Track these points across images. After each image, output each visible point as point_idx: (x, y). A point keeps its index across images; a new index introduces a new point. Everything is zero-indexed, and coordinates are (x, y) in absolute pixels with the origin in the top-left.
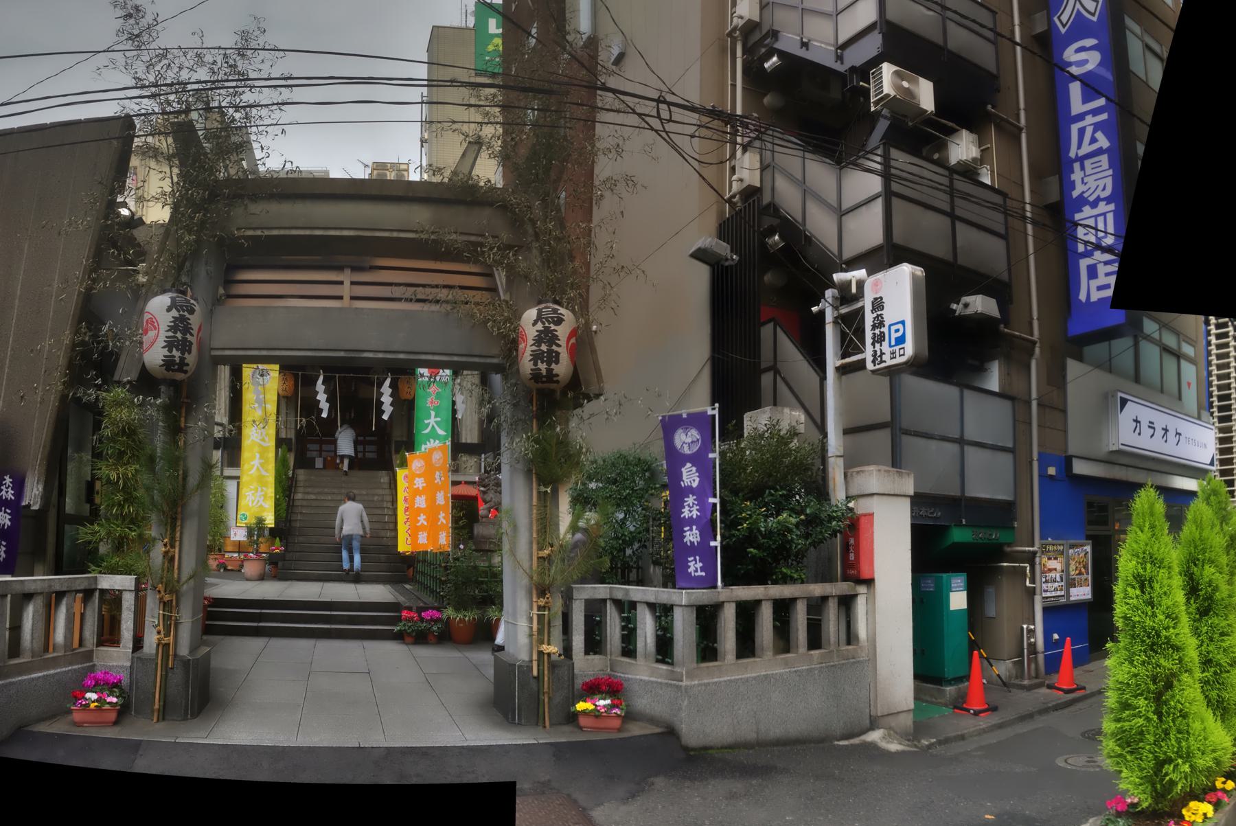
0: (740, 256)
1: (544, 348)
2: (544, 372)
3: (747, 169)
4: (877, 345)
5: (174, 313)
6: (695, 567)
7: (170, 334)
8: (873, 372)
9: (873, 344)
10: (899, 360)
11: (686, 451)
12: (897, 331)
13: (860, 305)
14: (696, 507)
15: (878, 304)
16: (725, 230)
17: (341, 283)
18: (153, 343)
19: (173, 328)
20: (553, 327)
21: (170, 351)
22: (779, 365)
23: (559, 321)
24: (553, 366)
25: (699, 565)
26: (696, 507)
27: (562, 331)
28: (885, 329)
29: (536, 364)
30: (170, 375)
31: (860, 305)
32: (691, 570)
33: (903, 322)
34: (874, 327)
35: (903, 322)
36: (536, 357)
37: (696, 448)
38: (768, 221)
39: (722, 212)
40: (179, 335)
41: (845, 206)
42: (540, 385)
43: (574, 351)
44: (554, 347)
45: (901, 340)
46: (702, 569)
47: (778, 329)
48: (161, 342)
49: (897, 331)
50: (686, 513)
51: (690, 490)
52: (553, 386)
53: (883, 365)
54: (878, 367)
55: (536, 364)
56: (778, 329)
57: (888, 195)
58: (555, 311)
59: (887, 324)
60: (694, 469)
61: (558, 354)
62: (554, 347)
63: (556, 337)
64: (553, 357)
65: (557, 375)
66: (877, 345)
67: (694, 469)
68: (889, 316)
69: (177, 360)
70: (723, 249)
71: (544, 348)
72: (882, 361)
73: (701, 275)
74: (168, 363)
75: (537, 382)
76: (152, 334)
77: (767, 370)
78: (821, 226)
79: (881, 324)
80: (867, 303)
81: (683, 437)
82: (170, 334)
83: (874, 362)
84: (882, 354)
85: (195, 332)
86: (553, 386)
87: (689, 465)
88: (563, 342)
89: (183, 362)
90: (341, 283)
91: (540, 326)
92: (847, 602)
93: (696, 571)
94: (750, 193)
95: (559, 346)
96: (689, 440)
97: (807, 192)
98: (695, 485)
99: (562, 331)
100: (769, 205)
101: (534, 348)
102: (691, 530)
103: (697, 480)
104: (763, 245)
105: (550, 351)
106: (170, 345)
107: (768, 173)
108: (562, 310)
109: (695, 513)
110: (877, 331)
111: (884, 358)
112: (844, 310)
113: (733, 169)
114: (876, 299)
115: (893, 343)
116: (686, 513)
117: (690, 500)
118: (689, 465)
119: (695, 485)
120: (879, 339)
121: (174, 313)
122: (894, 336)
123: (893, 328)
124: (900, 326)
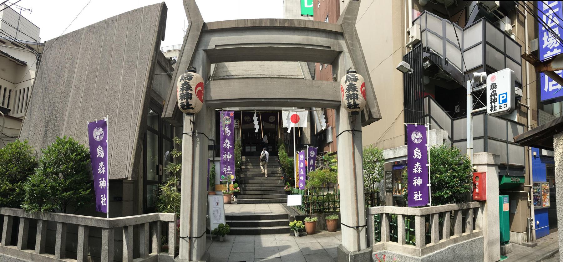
0: (414, 70)
1: (351, 92)
2: (353, 104)
3: (415, 33)
4: (493, 104)
6: (417, 196)
8: (490, 114)
9: (491, 103)
10: (503, 109)
11: (416, 142)
12: (503, 97)
13: (483, 87)
14: (420, 168)
15: (494, 86)
16: (405, 58)
20: (354, 83)
22: (431, 114)
23: (356, 80)
24: (356, 100)
25: (420, 195)
26: (420, 168)
27: (358, 84)
28: (497, 97)
29: (348, 101)
31: (483, 87)
32: (415, 198)
33: (506, 94)
34: (491, 96)
35: (506, 94)
36: (348, 97)
37: (420, 141)
38: (426, 55)
39: (403, 52)
41: (465, 48)
42: (352, 110)
43: (364, 94)
44: (355, 92)
45: (505, 101)
46: (421, 197)
47: (431, 100)
49: (503, 97)
50: (415, 171)
51: (417, 160)
52: (358, 110)
53: (496, 111)
54: (493, 112)
55: (348, 101)
56: (431, 100)
57: (485, 43)
58: (354, 76)
59: (498, 94)
60: (419, 150)
61: (191, 94)
62: (355, 92)
64: (355, 97)
65: (358, 105)
66: (493, 104)
68: (499, 91)
70: (408, 66)
71: (351, 92)
72: (495, 110)
73: (400, 74)
75: (350, 108)
77: (427, 116)
78: (453, 56)
79: (495, 94)
80: (488, 85)
83: (491, 110)
84: (495, 107)
86: (358, 110)
87: (417, 148)
88: (359, 89)
91: (348, 83)
92: (475, 211)
93: (418, 198)
94: (417, 43)
95: (357, 91)
96: (418, 137)
97: (445, 40)
98: (420, 158)
99: (358, 84)
100: (425, 48)
101: (347, 93)
102: (417, 179)
104: (421, 65)
105: (354, 94)
107: (424, 34)
108: (357, 75)
109: (420, 171)
110: (493, 98)
111: (496, 108)
112: (476, 89)
113: (409, 33)
114: (493, 84)
115: (501, 102)
116: (415, 171)
117: (418, 164)
118: (417, 148)
119: (420, 158)
120: (494, 101)
122: (501, 99)
123: (501, 96)
124: (505, 95)
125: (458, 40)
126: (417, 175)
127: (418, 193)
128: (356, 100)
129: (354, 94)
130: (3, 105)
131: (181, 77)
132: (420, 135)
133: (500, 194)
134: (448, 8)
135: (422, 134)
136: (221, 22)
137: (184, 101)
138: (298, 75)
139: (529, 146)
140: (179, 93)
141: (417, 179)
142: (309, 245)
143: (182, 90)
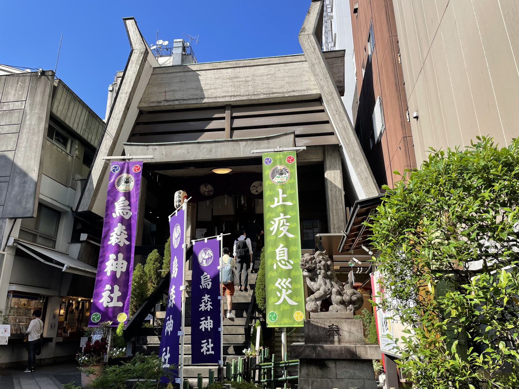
14: (209, 303)
17: (223, 118)
25: (211, 345)
26: (209, 303)
32: (204, 350)
50: (203, 307)
51: (206, 291)
90: (223, 118)
93: (208, 350)
98: (209, 287)
102: (206, 319)
109: (209, 307)
116: (203, 307)
117: (206, 297)
119: (209, 287)
125: (348, 118)
126: (206, 314)
127: (208, 342)
130: (223, 130)
133: (302, 248)
136: (355, 95)
138: (308, 89)
141: (206, 319)
142: (312, 15)
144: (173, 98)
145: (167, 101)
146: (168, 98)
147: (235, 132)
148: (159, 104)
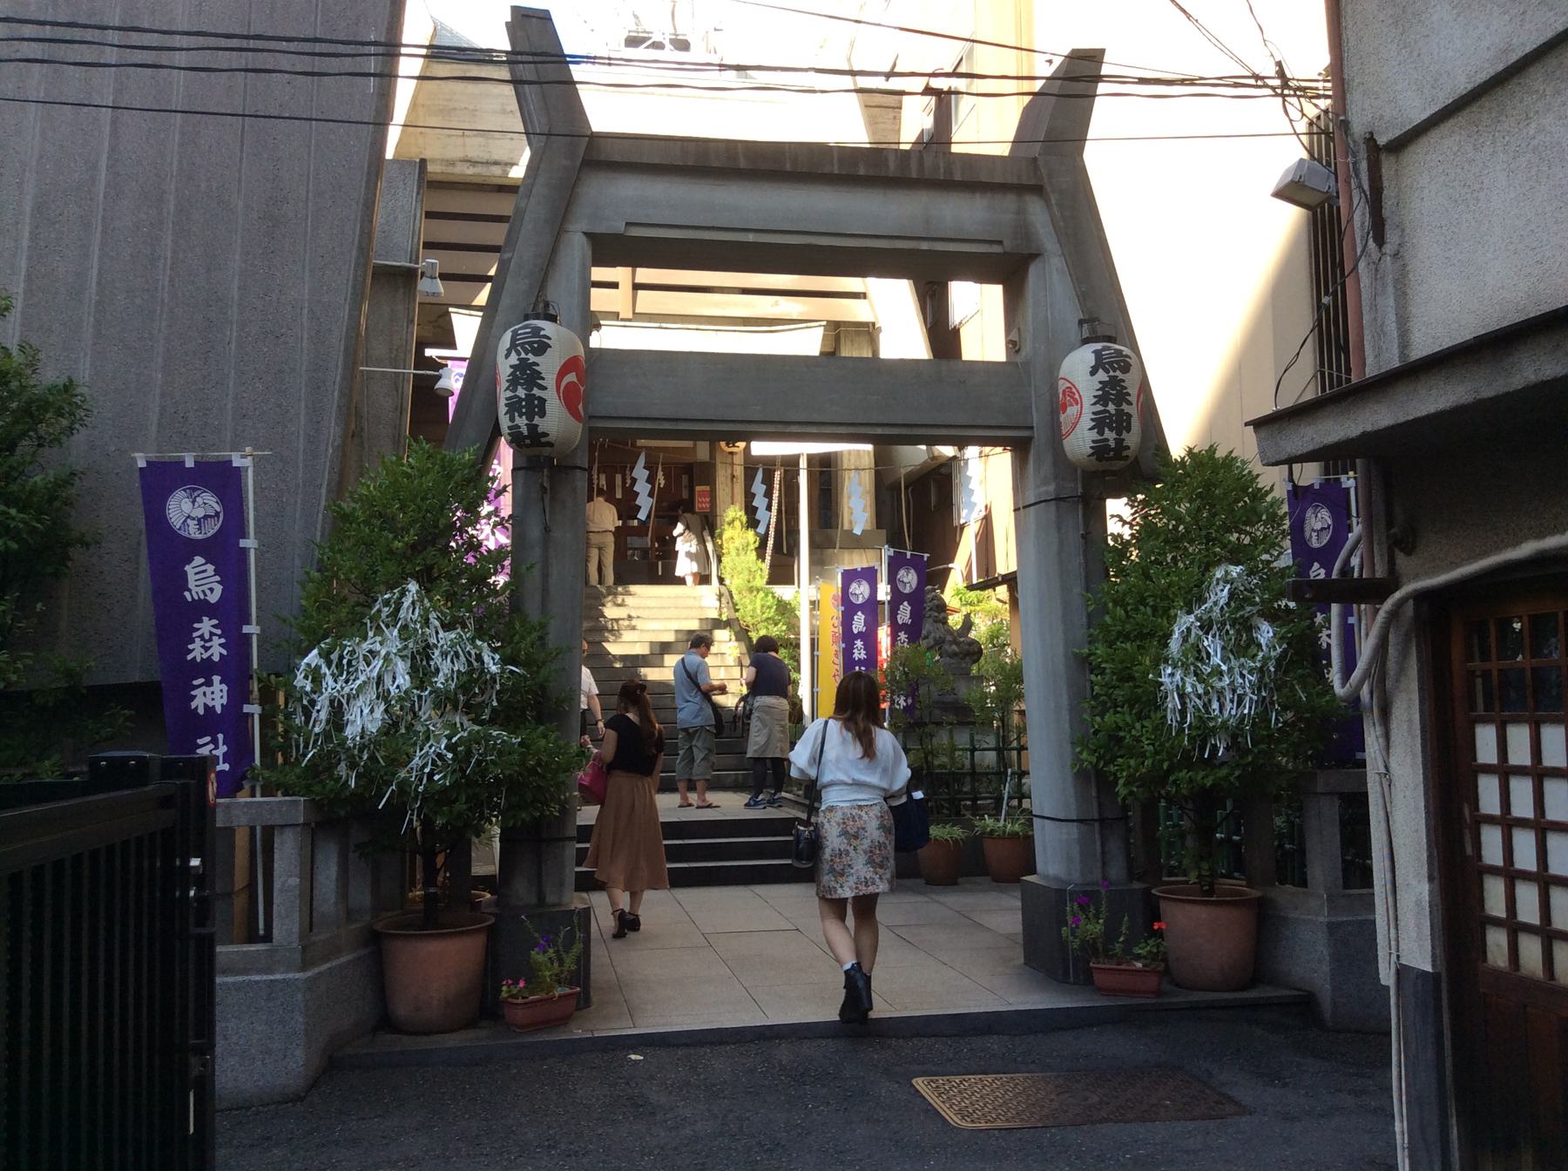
5: (1102, 375)
7: (1099, 408)
11: (193, 532)
18: (1075, 424)
19: (1102, 399)
20: (532, 358)
21: (1101, 433)
24: (537, 420)
26: (217, 641)
30: (1105, 465)
37: (212, 529)
40: (1111, 407)
44: (536, 391)
48: (1086, 421)
50: (197, 652)
60: (210, 568)
61: (542, 401)
62: (536, 391)
63: (538, 375)
65: (545, 435)
67: (210, 568)
69: (1112, 444)
71: (521, 392)
74: (1100, 450)
76: (1072, 411)
81: (186, 506)
82: (1099, 408)
85: (1133, 399)
87: (199, 560)
89: (1121, 445)
96: (200, 513)
98: (214, 598)
101: (509, 394)
102: (209, 683)
103: (219, 589)
105: (530, 397)
106: (1100, 423)
109: (217, 651)
116: (197, 652)
117: (206, 626)
118: (199, 560)
121: (1102, 375)
126: (206, 669)
127: (215, 741)
128: (537, 420)
129: (530, 397)
131: (508, 336)
132: (209, 502)
134: (437, 52)
135: (222, 499)
137: (522, 422)
139: (1359, 604)
140: (503, 395)
143: (513, 383)
144: (485, 157)
145: (474, 163)
146: (473, 154)
147: (640, 292)
148: (450, 170)
